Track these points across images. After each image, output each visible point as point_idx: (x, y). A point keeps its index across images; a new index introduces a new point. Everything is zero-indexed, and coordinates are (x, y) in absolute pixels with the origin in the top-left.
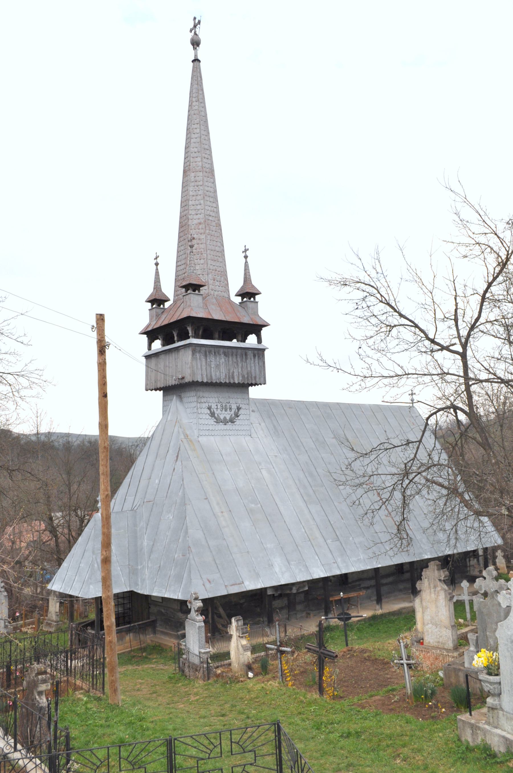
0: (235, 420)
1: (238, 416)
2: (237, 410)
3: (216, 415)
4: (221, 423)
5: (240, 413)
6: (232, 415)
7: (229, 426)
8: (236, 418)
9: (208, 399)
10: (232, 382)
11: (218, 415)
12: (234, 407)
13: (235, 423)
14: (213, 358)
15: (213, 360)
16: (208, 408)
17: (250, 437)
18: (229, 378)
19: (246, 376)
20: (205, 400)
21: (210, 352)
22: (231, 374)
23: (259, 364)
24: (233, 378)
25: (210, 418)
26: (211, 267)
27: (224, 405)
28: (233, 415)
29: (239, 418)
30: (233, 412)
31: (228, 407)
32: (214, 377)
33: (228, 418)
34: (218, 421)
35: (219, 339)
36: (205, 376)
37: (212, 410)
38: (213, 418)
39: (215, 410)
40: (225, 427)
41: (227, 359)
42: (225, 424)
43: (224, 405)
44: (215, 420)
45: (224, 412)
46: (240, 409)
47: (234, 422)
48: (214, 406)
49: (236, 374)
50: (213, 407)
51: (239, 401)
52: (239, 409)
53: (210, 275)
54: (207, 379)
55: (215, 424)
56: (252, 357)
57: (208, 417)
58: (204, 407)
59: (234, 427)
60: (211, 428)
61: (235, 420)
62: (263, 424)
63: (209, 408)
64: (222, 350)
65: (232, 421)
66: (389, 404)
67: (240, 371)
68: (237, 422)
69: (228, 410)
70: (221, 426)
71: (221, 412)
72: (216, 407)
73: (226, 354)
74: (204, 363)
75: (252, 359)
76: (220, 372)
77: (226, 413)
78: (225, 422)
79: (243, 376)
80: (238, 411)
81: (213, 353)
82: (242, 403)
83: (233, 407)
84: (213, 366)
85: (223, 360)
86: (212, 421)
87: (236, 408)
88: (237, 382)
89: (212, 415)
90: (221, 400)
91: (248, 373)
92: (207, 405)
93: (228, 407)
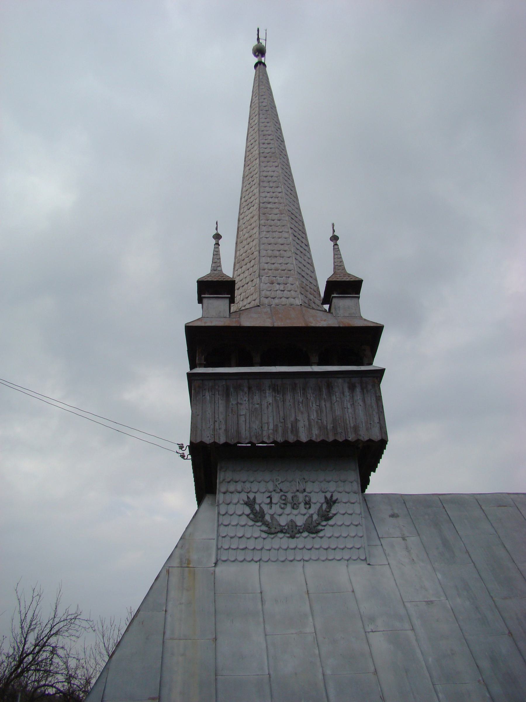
0: (320, 527)
1: (328, 519)
2: (325, 506)
3: (268, 518)
4: (281, 535)
5: (333, 511)
6: (311, 516)
7: (303, 540)
8: (324, 523)
9: (248, 485)
10: (291, 439)
11: (272, 516)
12: (318, 499)
13: (321, 534)
14: (244, 399)
15: (244, 403)
16: (246, 503)
17: (364, 566)
18: (285, 431)
19: (330, 426)
20: (239, 487)
21: (238, 388)
22: (289, 426)
23: (364, 401)
24: (295, 430)
25: (251, 523)
26: (266, 266)
27: (289, 496)
28: (315, 517)
29: (331, 522)
30: (314, 509)
31: (301, 500)
32: (245, 433)
33: (300, 521)
34: (272, 530)
35: (319, 364)
36: (222, 432)
37: (257, 507)
38: (259, 524)
39: (265, 508)
40: (293, 543)
41: (279, 397)
42: (293, 537)
43: (289, 496)
44: (264, 528)
45: (288, 509)
46: (335, 502)
47: (317, 532)
48: (261, 499)
49: (302, 425)
50: (258, 501)
51: (332, 487)
52: (330, 502)
53: (263, 278)
54: (227, 437)
55: (264, 535)
56: (346, 390)
57: (244, 520)
58: (235, 501)
59: (317, 543)
60: (251, 544)
61: (320, 527)
62: (413, 540)
63: (250, 503)
64: (267, 382)
65: (312, 529)
66: (346, 295)
67: (314, 416)
68: (328, 532)
69: (302, 505)
70: (281, 541)
71: (280, 511)
72: (268, 500)
73: (275, 389)
74: (222, 409)
75: (347, 393)
76: (261, 422)
77: (295, 512)
78: (292, 531)
79: (322, 428)
80: (330, 507)
81: (246, 389)
82: (340, 489)
83: (313, 500)
84: (243, 412)
85: (270, 400)
86: (257, 531)
87: (323, 500)
88: (304, 438)
89: (258, 516)
90: (284, 487)
91: (334, 420)
92: (244, 496)
93: (301, 500)
